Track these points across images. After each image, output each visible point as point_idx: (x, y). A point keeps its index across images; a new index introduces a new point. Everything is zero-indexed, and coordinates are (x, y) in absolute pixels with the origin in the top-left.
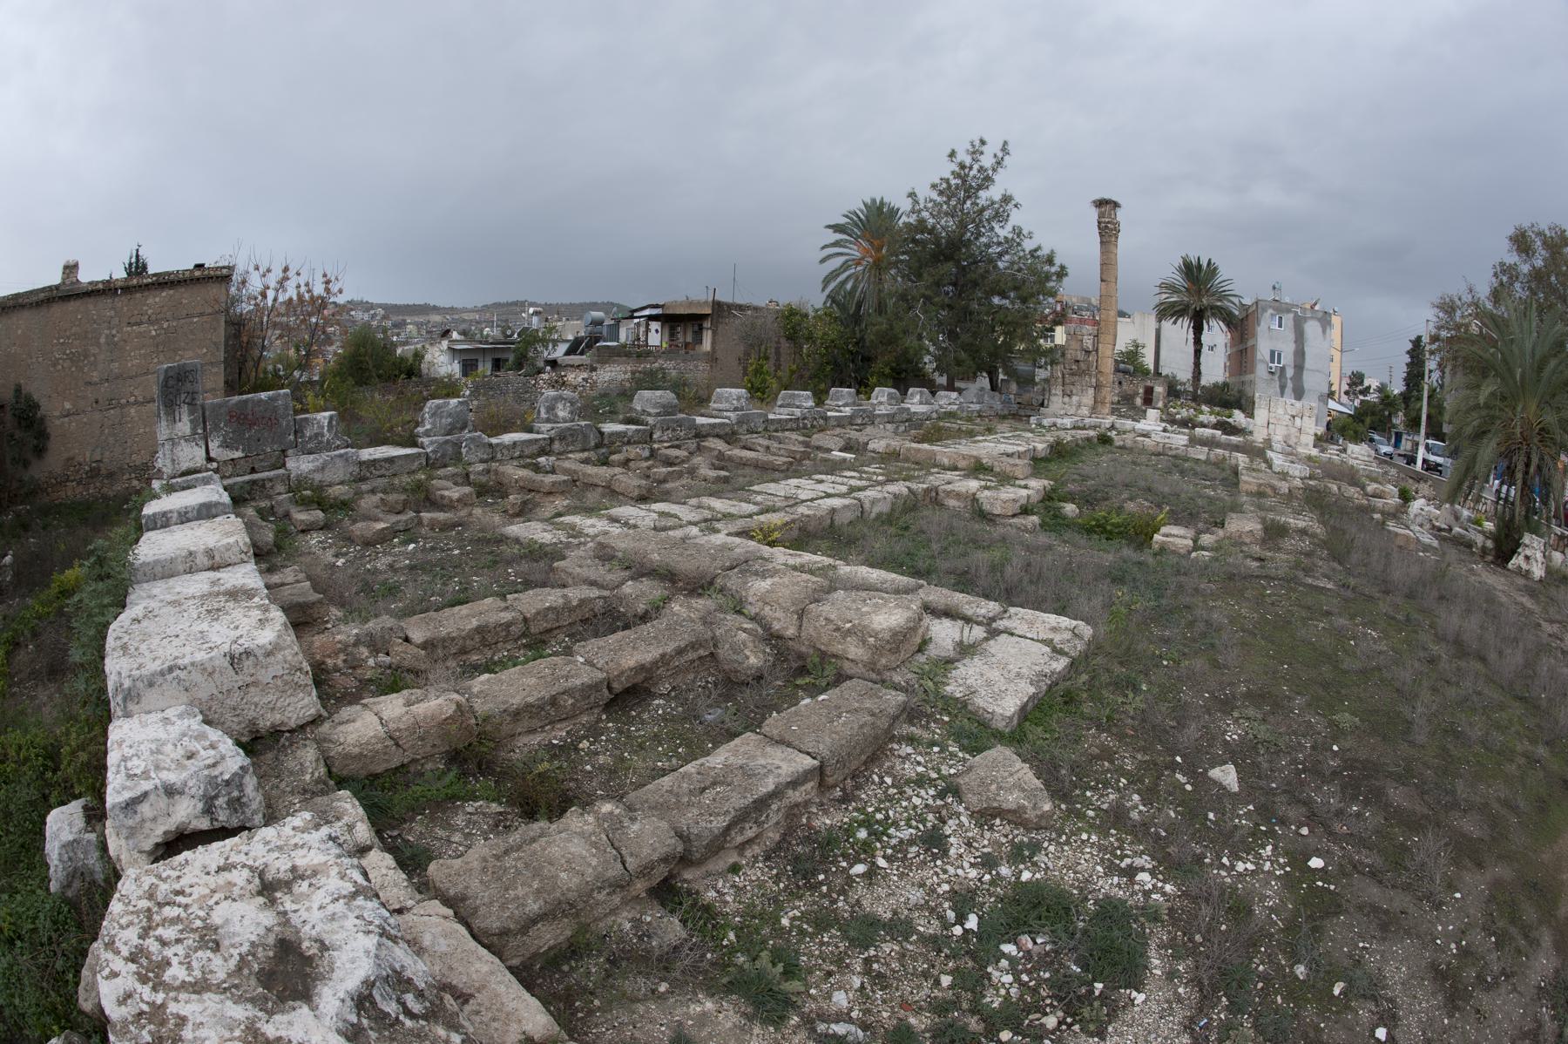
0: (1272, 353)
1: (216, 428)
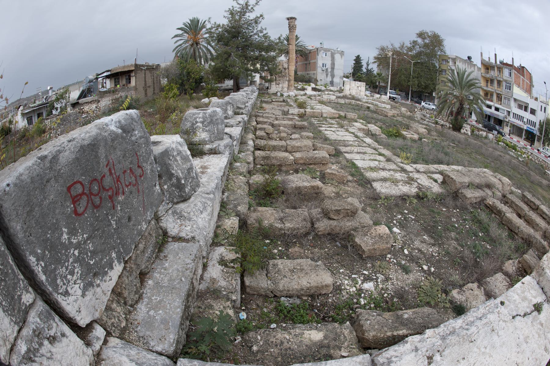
0: (323, 64)
1: (56, 253)
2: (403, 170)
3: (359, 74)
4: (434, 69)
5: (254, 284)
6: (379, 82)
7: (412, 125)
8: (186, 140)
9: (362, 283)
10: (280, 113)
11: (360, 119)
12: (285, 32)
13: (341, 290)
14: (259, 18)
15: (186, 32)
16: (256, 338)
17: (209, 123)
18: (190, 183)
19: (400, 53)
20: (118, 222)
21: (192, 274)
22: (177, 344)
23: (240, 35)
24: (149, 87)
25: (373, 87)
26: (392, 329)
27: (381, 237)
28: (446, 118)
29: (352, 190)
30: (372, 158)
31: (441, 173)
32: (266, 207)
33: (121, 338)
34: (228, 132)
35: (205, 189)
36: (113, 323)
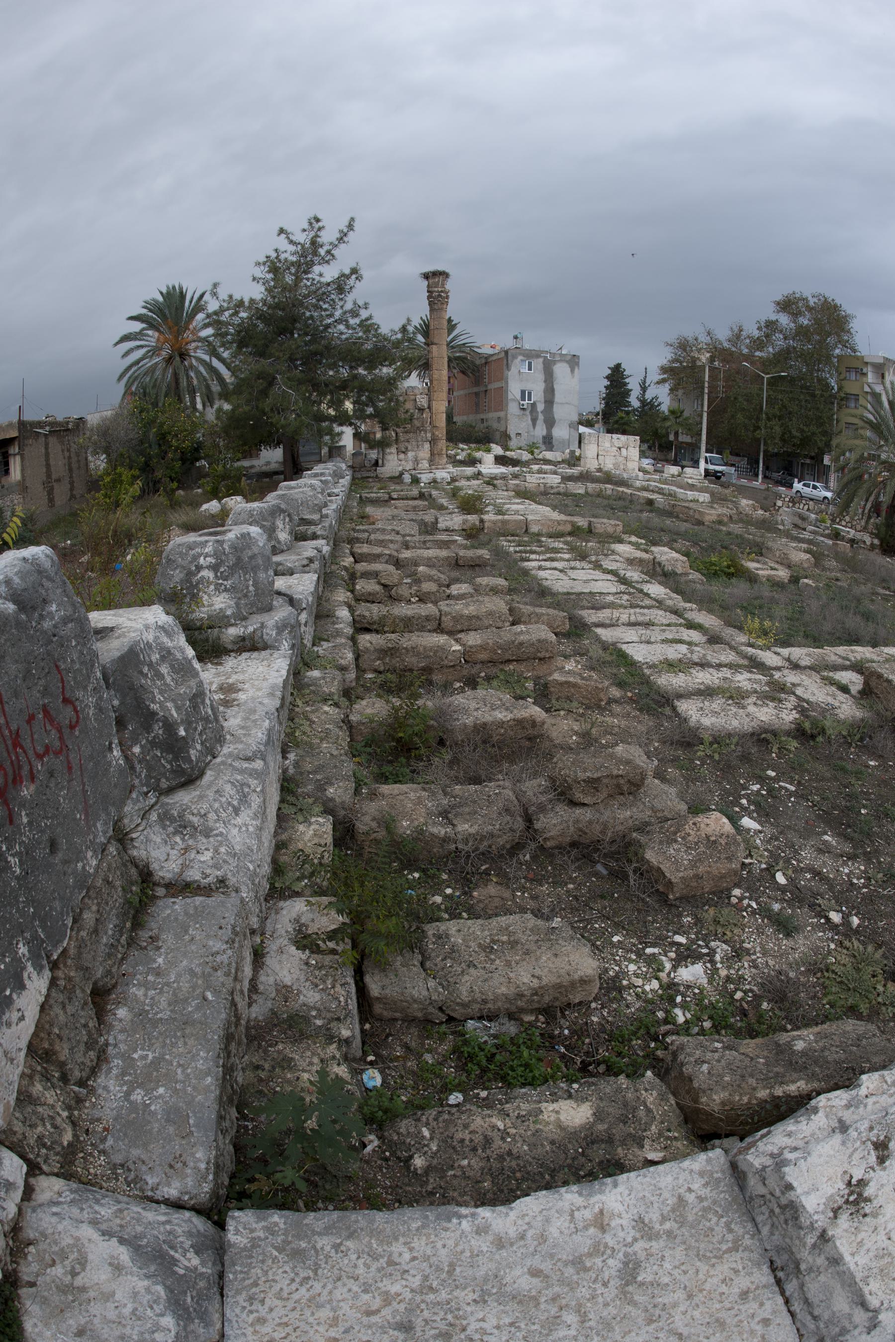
2: (756, 665)
3: (620, 414)
4: (826, 394)
5: (392, 992)
6: (676, 434)
7: (770, 544)
8: (178, 617)
9: (675, 968)
10: (414, 529)
11: (631, 533)
12: (418, 311)
13: (620, 989)
14: (348, 277)
15: (152, 325)
16: (419, 1136)
17: (233, 569)
18: (200, 734)
19: (732, 354)
20: (26, 856)
21: (231, 979)
22: (216, 1174)
23: (298, 325)
24: (58, 480)
25: (660, 446)
26: (767, 1082)
27: (711, 843)
28: (863, 523)
29: (623, 723)
30: (670, 637)
31: (858, 667)
32: (400, 782)
33: (66, 1175)
34: (283, 589)
35: (240, 746)
36: (40, 1138)
